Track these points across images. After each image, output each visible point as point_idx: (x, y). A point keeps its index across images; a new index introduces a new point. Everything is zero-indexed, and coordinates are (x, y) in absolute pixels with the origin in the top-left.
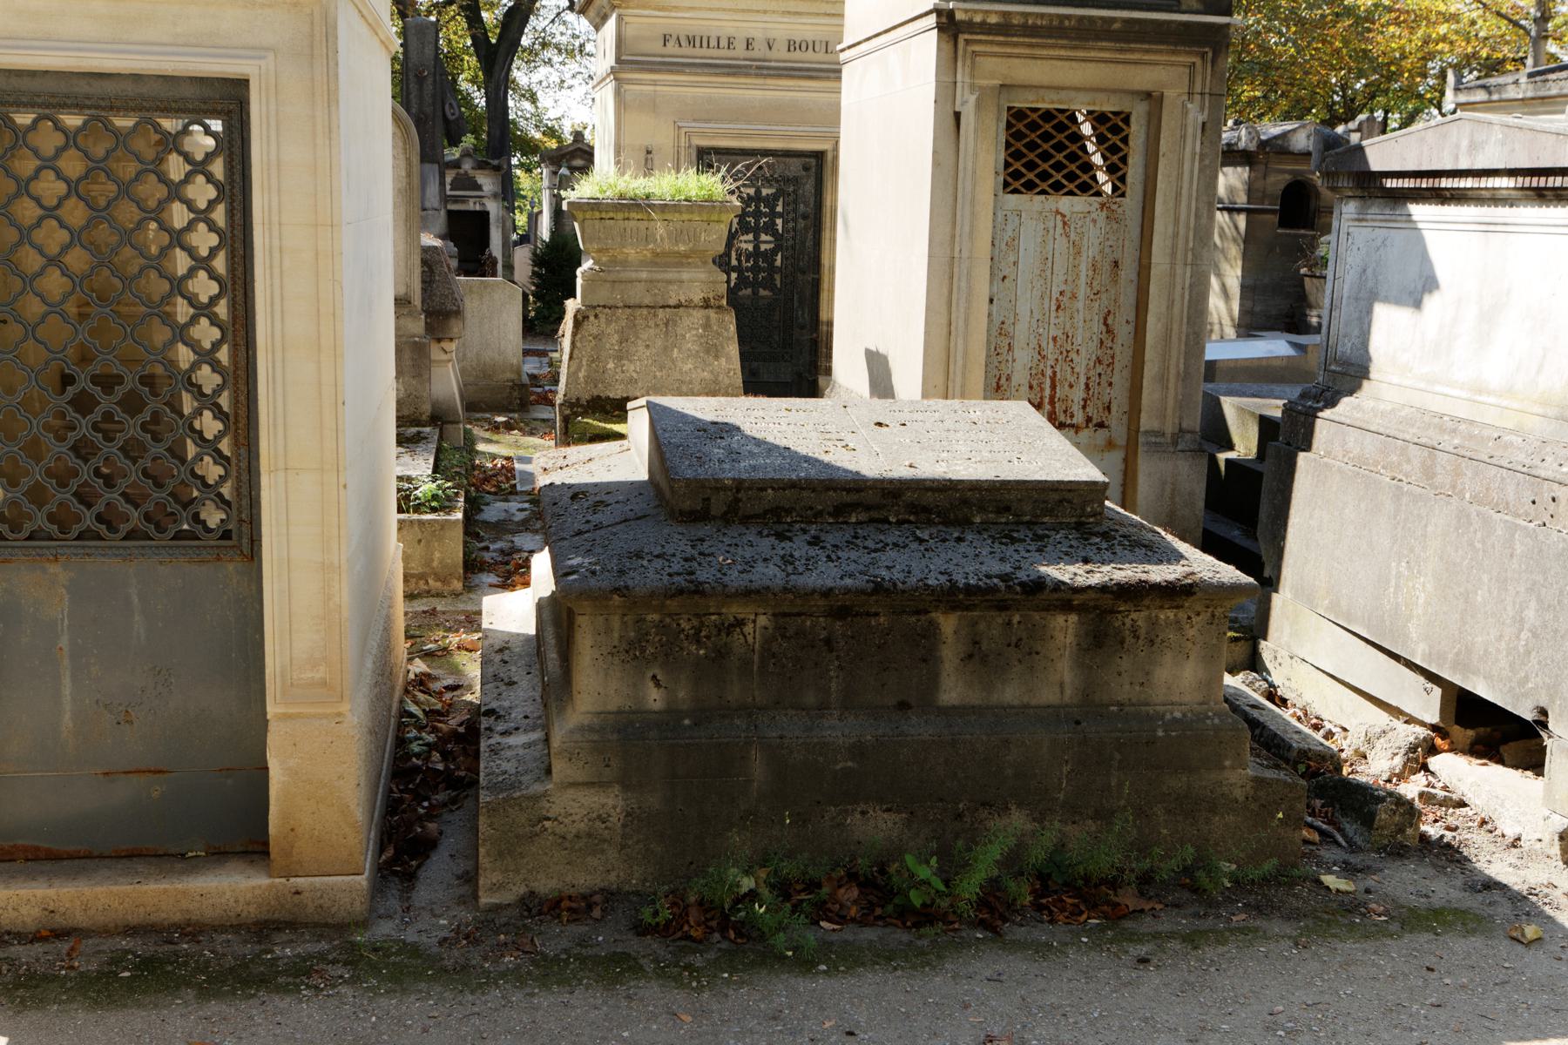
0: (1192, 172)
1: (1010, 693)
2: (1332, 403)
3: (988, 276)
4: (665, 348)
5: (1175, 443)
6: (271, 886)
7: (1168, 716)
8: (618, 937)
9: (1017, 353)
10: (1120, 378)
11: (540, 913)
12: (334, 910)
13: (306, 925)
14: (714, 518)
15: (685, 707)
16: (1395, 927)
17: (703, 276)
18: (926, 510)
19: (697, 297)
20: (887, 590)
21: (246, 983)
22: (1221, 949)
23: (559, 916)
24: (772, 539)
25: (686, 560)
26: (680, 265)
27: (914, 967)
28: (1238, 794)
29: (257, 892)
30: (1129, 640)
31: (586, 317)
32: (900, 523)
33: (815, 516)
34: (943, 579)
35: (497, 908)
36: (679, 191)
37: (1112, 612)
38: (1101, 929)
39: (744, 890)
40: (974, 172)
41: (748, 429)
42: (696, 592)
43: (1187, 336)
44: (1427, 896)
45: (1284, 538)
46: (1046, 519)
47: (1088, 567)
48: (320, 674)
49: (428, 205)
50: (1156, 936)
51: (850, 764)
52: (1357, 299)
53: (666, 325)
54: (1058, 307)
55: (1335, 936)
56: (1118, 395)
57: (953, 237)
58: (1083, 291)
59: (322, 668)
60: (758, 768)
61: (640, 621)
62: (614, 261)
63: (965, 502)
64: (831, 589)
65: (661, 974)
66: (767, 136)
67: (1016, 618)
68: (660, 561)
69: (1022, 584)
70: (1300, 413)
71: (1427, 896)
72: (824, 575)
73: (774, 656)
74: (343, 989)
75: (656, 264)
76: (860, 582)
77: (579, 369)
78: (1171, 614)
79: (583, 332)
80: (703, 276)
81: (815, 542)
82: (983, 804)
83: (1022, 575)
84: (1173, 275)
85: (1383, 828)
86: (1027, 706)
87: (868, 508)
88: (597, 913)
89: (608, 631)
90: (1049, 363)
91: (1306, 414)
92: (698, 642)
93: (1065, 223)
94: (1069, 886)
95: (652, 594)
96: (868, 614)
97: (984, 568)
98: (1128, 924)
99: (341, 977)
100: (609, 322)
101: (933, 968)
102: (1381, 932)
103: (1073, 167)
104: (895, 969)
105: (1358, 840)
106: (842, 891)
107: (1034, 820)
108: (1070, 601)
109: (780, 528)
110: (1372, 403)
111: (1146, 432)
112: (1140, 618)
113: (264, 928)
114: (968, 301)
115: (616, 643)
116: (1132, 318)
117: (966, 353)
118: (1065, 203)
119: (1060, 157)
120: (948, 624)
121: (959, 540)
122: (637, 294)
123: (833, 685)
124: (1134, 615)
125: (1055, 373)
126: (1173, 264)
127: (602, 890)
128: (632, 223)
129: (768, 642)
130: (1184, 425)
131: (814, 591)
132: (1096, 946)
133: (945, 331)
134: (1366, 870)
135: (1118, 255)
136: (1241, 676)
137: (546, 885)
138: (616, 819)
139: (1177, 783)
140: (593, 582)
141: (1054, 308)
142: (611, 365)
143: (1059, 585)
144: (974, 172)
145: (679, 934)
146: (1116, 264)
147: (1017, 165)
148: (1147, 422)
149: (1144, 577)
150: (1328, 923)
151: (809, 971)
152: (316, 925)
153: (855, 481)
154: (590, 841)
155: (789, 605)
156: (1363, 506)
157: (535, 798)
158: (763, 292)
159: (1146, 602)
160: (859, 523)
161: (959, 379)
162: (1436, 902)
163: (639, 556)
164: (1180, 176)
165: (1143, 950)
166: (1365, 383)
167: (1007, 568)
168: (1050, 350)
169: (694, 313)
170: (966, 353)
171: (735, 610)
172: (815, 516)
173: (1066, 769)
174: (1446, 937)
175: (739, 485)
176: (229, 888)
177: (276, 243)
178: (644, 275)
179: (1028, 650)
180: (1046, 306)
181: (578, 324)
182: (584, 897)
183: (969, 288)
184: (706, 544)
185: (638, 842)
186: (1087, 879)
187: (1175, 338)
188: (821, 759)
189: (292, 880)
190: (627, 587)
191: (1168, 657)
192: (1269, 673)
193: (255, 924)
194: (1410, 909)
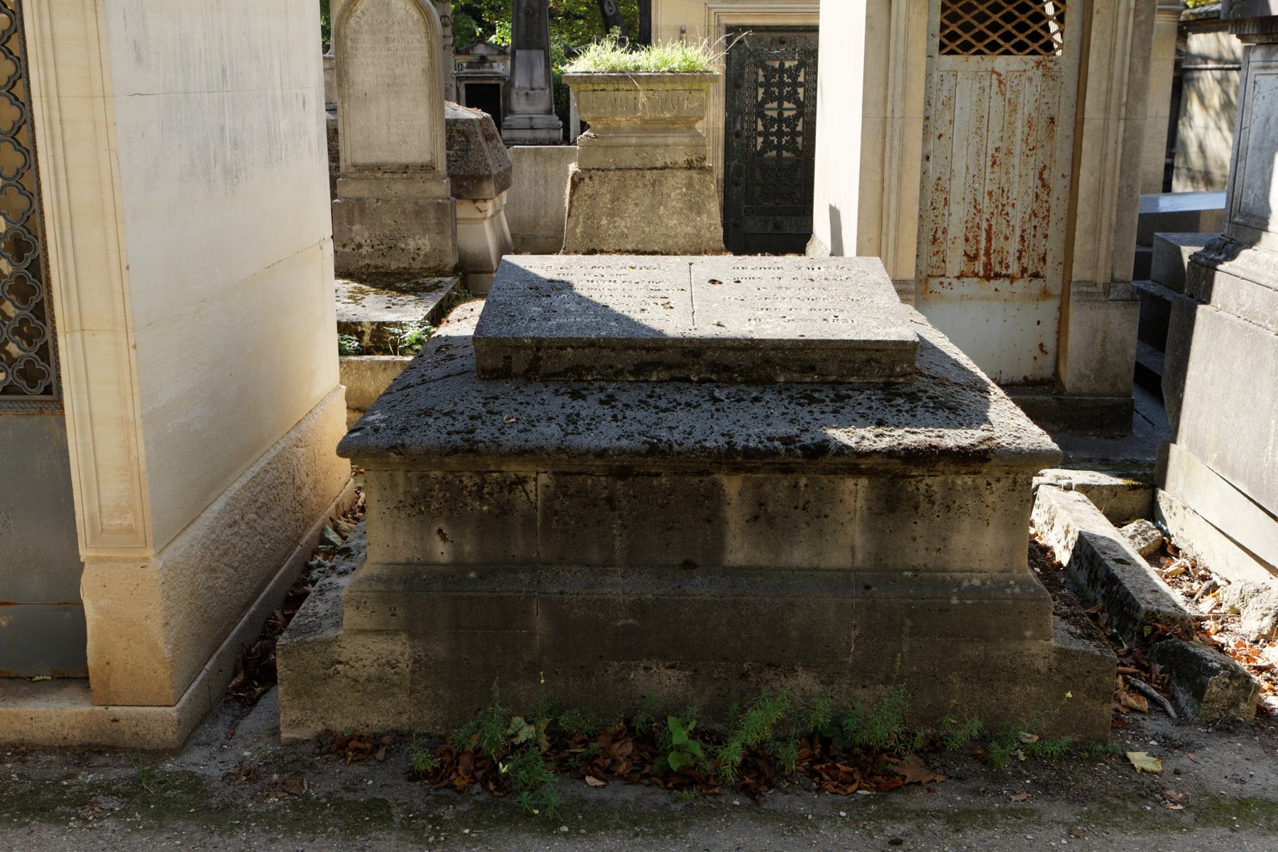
0: (1126, 28)
1: (799, 556)
2: (1232, 256)
3: (920, 134)
4: (653, 206)
5: (1107, 292)
6: (92, 713)
7: (966, 584)
8: (389, 781)
9: (953, 207)
10: (1056, 231)
11: (329, 752)
12: (149, 737)
13: (125, 750)
14: (516, 376)
15: (471, 560)
16: (1188, 818)
17: (686, 140)
18: (727, 369)
19: (681, 159)
20: (662, 452)
21: (25, 810)
22: (985, 834)
23: (345, 756)
24: (566, 397)
25: (472, 418)
26: (667, 130)
27: (655, 835)
28: (1040, 664)
29: (80, 718)
30: (924, 505)
31: (582, 179)
32: (702, 381)
33: (616, 374)
34: (722, 441)
35: (294, 743)
36: (666, 63)
37: (904, 476)
38: (867, 801)
39: (522, 738)
40: (907, 34)
41: (582, 288)
42: (471, 451)
43: (1120, 189)
44: (1243, 782)
45: (1182, 390)
46: (853, 379)
47: (880, 430)
48: (128, 520)
49: (535, 85)
50: (922, 814)
51: (631, 621)
52: (1260, 149)
53: (653, 185)
54: (994, 163)
55: (1116, 825)
56: (1054, 246)
57: (886, 97)
58: (1018, 147)
59: (130, 516)
60: (540, 623)
61: (423, 477)
62: (607, 129)
63: (768, 361)
64: (605, 450)
65: (406, 826)
66: (788, 14)
67: (803, 481)
68: (446, 419)
69: (804, 448)
70: (1202, 265)
71: (1243, 782)
72: (605, 435)
73: (556, 513)
74: (109, 824)
75: (645, 130)
76: (637, 443)
77: (576, 226)
78: (969, 480)
79: (579, 193)
80: (686, 140)
81: (609, 401)
82: (769, 665)
83: (806, 439)
84: (1106, 129)
85: (1213, 701)
86: (816, 569)
87: (669, 367)
88: (380, 755)
89: (394, 486)
90: (985, 216)
91: (1208, 267)
92: (481, 498)
93: (1000, 82)
94: (849, 755)
95: (428, 452)
96: (650, 475)
97: (770, 430)
98: (897, 798)
99: (112, 810)
100: (602, 183)
101: (675, 836)
102: (1173, 823)
103: (1009, 27)
104: (637, 835)
105: (1189, 711)
106: (617, 745)
107: (822, 682)
108: (856, 465)
109: (577, 386)
110: (1267, 256)
111: (1078, 282)
112: (935, 483)
113: (86, 752)
114: (901, 158)
115: (402, 497)
116: (1067, 172)
117: (899, 210)
118: (1001, 63)
119: (996, 18)
120: (732, 486)
121: (756, 399)
122: (628, 158)
123: (617, 544)
124: (928, 481)
125: (990, 226)
126: (1106, 119)
127: (393, 731)
128: (621, 94)
129: (549, 499)
130: (1117, 276)
131: (588, 452)
132: (853, 823)
133: (878, 188)
134: (1185, 747)
135: (1053, 112)
136: (1131, 528)
137: (341, 724)
138: (404, 665)
139: (974, 651)
140: (372, 440)
141: (989, 163)
142: (604, 222)
143: (843, 449)
144: (907, 34)
145: (445, 782)
146: (1052, 120)
147: (954, 27)
148: (1078, 272)
149: (935, 441)
150: (1114, 810)
151: (550, 831)
152: (134, 750)
153: (654, 340)
154: (381, 685)
155: (568, 464)
156: (1249, 360)
157: (327, 643)
158: (785, 154)
159: (940, 467)
160: (660, 382)
161: (892, 233)
162: (1250, 789)
163: (428, 413)
164: (1114, 32)
165: (899, 829)
166: (1264, 236)
167: (794, 430)
168: (986, 205)
169: (679, 173)
170: (899, 210)
171: (514, 469)
172: (616, 374)
173: (854, 633)
174: (1243, 835)
175: (539, 344)
176: (53, 714)
177: (56, 115)
178: (633, 141)
179: (816, 513)
180: (982, 162)
181: (575, 185)
182: (376, 736)
183: (902, 146)
184: (498, 403)
185: (426, 688)
186: (867, 749)
187: (1107, 192)
188: (602, 616)
189: (111, 708)
190: (403, 445)
191: (966, 524)
192: (1164, 522)
193: (81, 746)
194: (1214, 798)
